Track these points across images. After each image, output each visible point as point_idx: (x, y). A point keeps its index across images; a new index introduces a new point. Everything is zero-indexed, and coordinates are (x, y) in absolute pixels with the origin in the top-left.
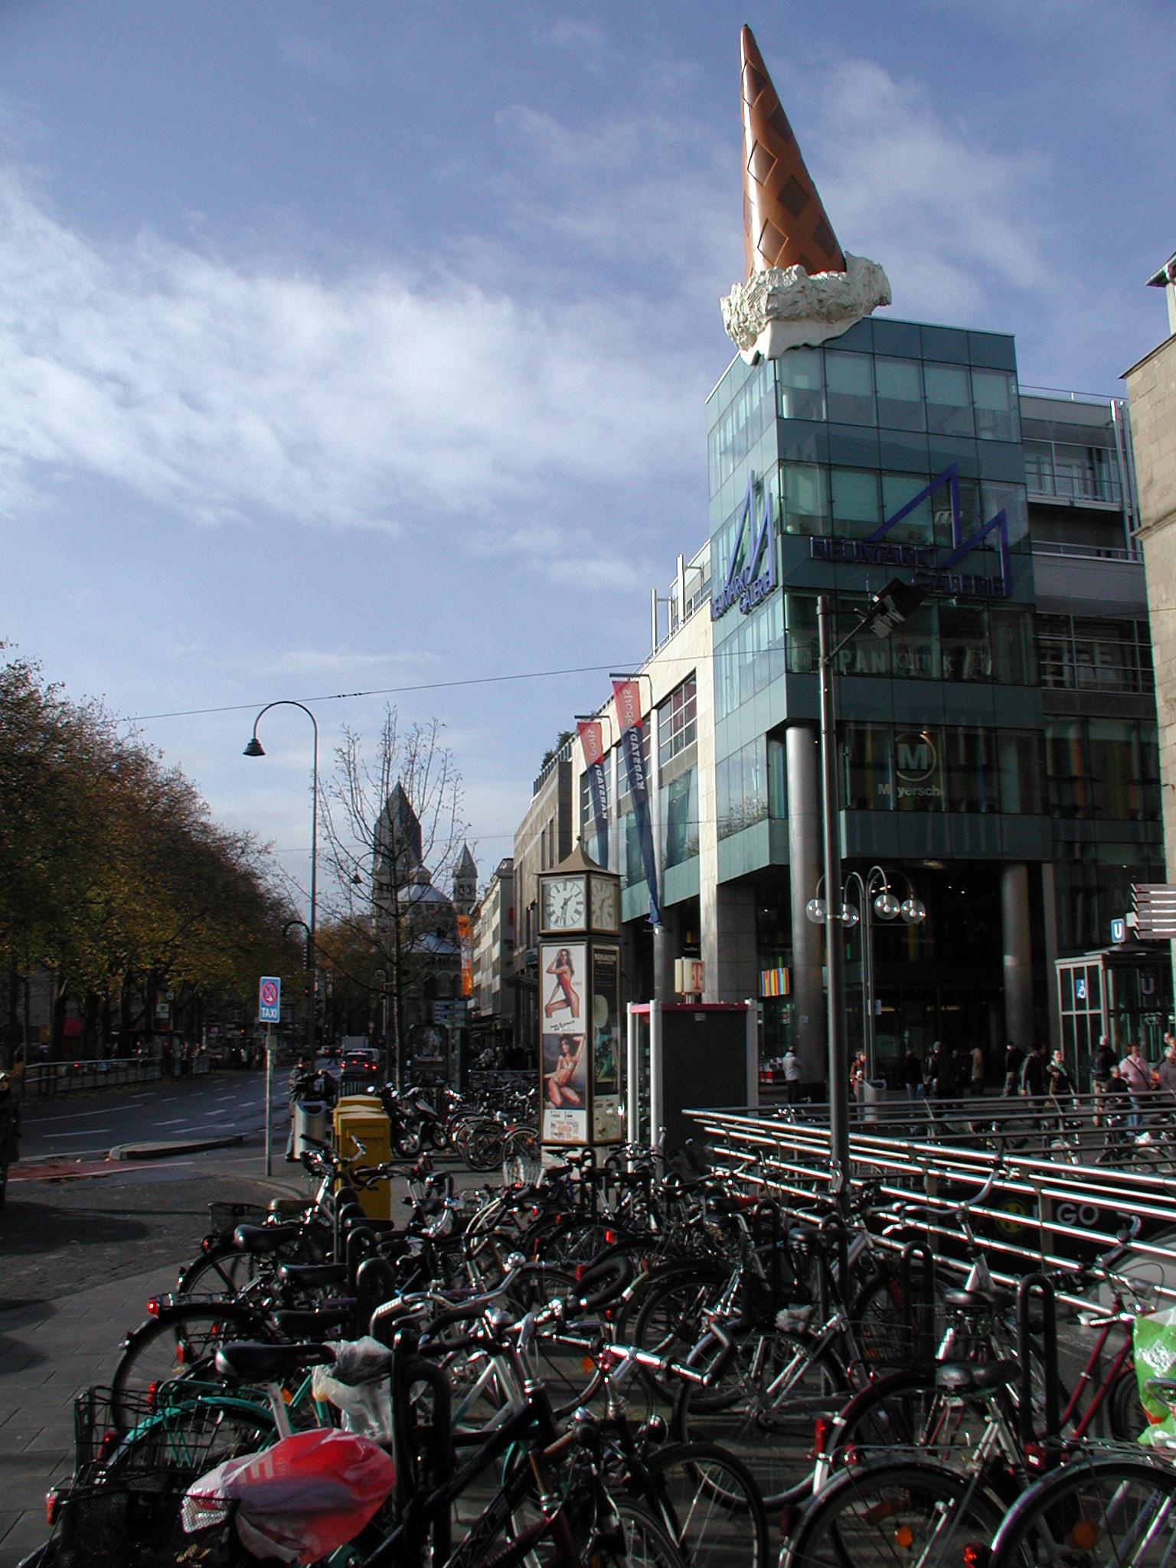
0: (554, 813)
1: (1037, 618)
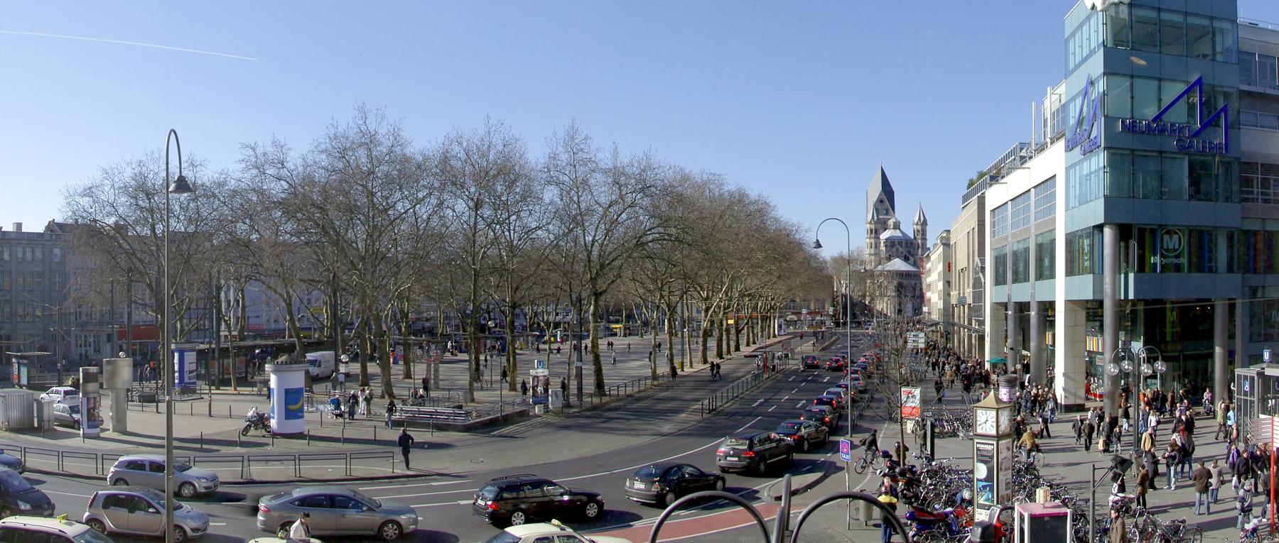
0: (974, 223)
1: (1240, 163)
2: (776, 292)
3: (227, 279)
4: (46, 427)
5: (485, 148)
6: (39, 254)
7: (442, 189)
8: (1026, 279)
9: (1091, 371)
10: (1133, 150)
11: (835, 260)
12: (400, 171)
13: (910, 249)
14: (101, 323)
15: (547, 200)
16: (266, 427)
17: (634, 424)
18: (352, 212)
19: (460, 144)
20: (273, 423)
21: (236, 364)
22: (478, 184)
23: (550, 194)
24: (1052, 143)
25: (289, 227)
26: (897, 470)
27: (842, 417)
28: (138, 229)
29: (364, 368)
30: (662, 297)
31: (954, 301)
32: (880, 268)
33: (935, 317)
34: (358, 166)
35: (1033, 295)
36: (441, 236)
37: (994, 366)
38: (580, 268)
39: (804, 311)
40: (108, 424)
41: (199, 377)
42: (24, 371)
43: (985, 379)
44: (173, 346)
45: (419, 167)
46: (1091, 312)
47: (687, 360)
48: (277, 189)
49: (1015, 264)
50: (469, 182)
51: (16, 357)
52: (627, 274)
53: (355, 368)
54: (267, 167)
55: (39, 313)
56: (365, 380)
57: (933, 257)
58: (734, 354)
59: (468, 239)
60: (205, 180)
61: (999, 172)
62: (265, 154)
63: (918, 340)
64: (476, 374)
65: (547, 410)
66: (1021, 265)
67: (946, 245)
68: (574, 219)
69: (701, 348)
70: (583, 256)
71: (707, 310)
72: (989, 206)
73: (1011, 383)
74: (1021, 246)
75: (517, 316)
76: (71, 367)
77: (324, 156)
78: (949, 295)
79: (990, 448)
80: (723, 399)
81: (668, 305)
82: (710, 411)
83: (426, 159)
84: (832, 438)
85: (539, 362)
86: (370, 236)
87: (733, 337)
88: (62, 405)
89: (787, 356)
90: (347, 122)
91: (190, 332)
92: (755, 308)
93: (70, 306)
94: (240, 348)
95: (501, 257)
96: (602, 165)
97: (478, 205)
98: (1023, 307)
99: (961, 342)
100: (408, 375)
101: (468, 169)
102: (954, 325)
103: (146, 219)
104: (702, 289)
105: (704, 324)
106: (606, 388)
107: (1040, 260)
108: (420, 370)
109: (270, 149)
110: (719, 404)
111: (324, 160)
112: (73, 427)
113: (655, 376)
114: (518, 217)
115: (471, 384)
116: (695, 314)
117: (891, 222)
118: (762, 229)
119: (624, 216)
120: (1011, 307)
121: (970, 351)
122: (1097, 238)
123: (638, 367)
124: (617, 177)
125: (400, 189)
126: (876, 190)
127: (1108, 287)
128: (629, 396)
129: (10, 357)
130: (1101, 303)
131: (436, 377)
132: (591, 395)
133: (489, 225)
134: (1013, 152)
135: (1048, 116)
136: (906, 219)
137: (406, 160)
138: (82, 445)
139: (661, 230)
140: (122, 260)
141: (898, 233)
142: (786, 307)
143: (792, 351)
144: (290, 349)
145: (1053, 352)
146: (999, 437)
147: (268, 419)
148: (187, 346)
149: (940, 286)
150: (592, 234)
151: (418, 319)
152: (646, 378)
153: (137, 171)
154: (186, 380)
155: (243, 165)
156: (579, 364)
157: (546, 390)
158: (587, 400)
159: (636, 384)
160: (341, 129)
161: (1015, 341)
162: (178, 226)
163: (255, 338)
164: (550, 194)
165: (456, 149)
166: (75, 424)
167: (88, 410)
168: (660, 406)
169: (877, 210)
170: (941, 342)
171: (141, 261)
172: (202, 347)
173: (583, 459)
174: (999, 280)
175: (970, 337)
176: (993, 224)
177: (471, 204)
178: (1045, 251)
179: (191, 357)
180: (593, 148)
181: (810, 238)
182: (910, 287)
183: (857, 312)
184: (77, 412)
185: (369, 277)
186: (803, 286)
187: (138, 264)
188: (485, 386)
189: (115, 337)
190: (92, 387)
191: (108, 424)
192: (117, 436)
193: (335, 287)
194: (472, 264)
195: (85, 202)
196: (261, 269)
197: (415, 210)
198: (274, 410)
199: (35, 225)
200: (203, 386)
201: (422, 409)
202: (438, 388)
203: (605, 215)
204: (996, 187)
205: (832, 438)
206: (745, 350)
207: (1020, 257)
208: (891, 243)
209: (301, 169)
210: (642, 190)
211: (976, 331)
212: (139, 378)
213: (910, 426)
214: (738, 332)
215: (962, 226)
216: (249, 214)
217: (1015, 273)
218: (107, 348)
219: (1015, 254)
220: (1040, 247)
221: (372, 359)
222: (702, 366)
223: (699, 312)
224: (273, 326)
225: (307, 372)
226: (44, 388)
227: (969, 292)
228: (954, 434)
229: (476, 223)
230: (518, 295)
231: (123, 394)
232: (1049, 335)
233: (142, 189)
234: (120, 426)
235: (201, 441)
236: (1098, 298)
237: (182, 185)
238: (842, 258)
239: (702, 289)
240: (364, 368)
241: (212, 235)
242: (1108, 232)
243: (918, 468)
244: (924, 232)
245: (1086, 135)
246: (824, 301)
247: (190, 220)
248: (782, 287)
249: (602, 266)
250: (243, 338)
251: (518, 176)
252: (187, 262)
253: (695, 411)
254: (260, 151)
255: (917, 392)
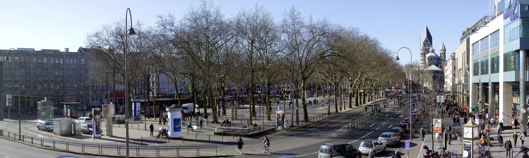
0: (465, 49)
2: (380, 79)
3: (152, 72)
4: (77, 133)
5: (255, 18)
6: (75, 62)
7: (237, 35)
8: (487, 73)
9: (515, 111)
11: (406, 66)
12: (220, 28)
13: (439, 61)
14: (103, 90)
15: (283, 40)
16: (167, 135)
17: (321, 133)
18: (199, 45)
19: (245, 16)
20: (169, 133)
21: (155, 109)
22: (253, 32)
23: (284, 37)
24: (498, 15)
25: (175, 51)
26: (430, 154)
27: (407, 132)
28: (118, 51)
29: (205, 111)
30: (332, 80)
31: (456, 82)
32: (426, 69)
33: (449, 90)
34: (202, 25)
35: (490, 80)
36: (238, 56)
37: (473, 110)
38: (296, 68)
39: (393, 87)
40: (104, 133)
41: (142, 113)
42: (69, 110)
43: (471, 115)
44: (132, 100)
45: (228, 26)
46: (514, 87)
47: (343, 107)
48: (171, 35)
49: (482, 66)
50: (249, 32)
51: (66, 104)
52: (317, 70)
53: (202, 110)
54: (166, 25)
55: (75, 86)
56: (206, 116)
57: (448, 64)
58: (363, 105)
59: (248, 56)
60: (143, 30)
61: (475, 29)
62: (166, 20)
63: (441, 99)
64: (253, 113)
65: (283, 129)
66: (485, 67)
67: (454, 59)
68: (295, 47)
69: (349, 101)
70: (298, 63)
71: (351, 85)
72: (472, 42)
73: (480, 117)
74: (485, 59)
75: (271, 89)
76: (89, 109)
77: (188, 21)
78: (454, 80)
79: (469, 144)
80: (357, 124)
81: (335, 83)
82: (352, 128)
83: (231, 22)
84: (401, 141)
85: (280, 108)
86: (207, 55)
87: (362, 97)
88: (84, 125)
89: (385, 106)
90: (197, 8)
91: (139, 94)
92: (372, 86)
93: (89, 82)
94: (158, 101)
95: (263, 63)
96: (306, 24)
97: (253, 42)
98: (486, 85)
99: (460, 100)
100: (224, 113)
101: (248, 26)
102: (456, 92)
103: (121, 47)
104: (350, 77)
105: (350, 91)
106: (309, 119)
107: (493, 65)
108: (229, 111)
109: (168, 18)
110: (356, 125)
111: (188, 23)
112: (89, 134)
113: (329, 113)
114: (271, 47)
115: (251, 117)
116: (347, 87)
117: (430, 50)
118: (375, 52)
119: (315, 46)
120: (480, 85)
121: (463, 104)
122: (517, 55)
123: (322, 110)
124: (312, 29)
125: (220, 35)
126: (424, 36)
128: (318, 122)
129: (63, 104)
130: (519, 83)
131: (236, 114)
132: (302, 122)
133: (258, 50)
134: (482, 20)
135: (496, 4)
136: (437, 48)
137: (222, 23)
138: (93, 141)
139: (331, 51)
140: (111, 64)
141: (433, 54)
142: (385, 86)
143: (387, 104)
144: (176, 102)
145: (498, 104)
146: (473, 139)
147: (167, 131)
148: (137, 100)
149: (451, 76)
150: (302, 53)
151: (229, 90)
152: (325, 114)
153: (117, 26)
154: (137, 115)
155: (158, 24)
156: (297, 108)
157: (283, 120)
158: (300, 123)
159: (321, 117)
160: (195, 10)
161: (482, 99)
162: (132, 49)
163: (163, 97)
164: (284, 37)
165: (243, 18)
166: (90, 133)
167: (96, 126)
168: (331, 126)
169: (425, 45)
170: (451, 99)
171: (119, 64)
172: (143, 101)
173: (305, 147)
174: (476, 73)
175: (463, 98)
176: (473, 50)
177: (250, 41)
178: (495, 61)
179: (138, 105)
180: (302, 17)
181: (395, 56)
182: (438, 77)
183: (416, 86)
184: (91, 128)
185: (207, 72)
186: (392, 76)
187: (118, 66)
188: (257, 118)
189: (109, 96)
190: (98, 117)
191: (104, 133)
192: (108, 137)
193: (193, 76)
194: (252, 68)
195: (95, 39)
196: (165, 69)
197: (225, 44)
198: (169, 126)
199: (74, 49)
200: (143, 117)
201: (229, 128)
202: (237, 119)
203: (307, 45)
204: (474, 34)
205: (401, 141)
206: (367, 103)
207: (484, 64)
208: (431, 58)
209: (180, 27)
210: (323, 34)
211: (465, 95)
212: (117, 111)
213: (437, 135)
214: (365, 95)
215: (460, 50)
216: (159, 45)
217: (482, 70)
218: (105, 101)
219: (482, 63)
220: (493, 59)
221: (209, 107)
222: (349, 109)
223: (348, 86)
224: (170, 93)
225: (182, 112)
226: (77, 118)
227: (463, 79)
228: (456, 139)
229: (252, 49)
230: (272, 79)
231: (111, 120)
232: (496, 97)
233: (119, 34)
234: (110, 133)
235: (142, 140)
236: (517, 81)
237: (132, 31)
238: (409, 65)
239: (350, 77)
240: (205, 111)
241: (146, 53)
242: (521, 53)
243: (439, 153)
244: (444, 54)
245: (512, 12)
246: (402, 84)
247: (138, 47)
248: (383, 77)
249: (306, 67)
250: (158, 97)
251: (270, 29)
252: (137, 64)
253: (346, 128)
254: (164, 19)
255: (440, 121)
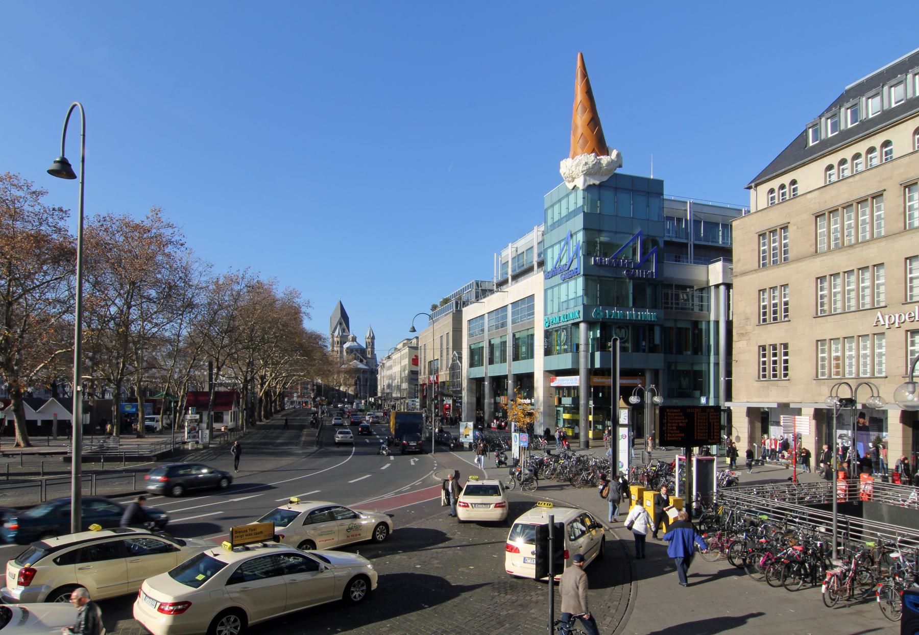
10: (599, 277)
117: (350, 337)
127: (582, 361)
208: (350, 350)
